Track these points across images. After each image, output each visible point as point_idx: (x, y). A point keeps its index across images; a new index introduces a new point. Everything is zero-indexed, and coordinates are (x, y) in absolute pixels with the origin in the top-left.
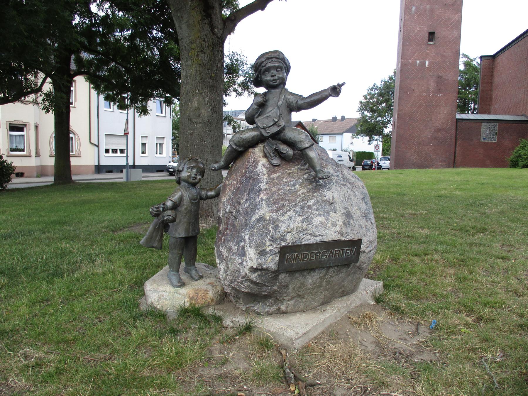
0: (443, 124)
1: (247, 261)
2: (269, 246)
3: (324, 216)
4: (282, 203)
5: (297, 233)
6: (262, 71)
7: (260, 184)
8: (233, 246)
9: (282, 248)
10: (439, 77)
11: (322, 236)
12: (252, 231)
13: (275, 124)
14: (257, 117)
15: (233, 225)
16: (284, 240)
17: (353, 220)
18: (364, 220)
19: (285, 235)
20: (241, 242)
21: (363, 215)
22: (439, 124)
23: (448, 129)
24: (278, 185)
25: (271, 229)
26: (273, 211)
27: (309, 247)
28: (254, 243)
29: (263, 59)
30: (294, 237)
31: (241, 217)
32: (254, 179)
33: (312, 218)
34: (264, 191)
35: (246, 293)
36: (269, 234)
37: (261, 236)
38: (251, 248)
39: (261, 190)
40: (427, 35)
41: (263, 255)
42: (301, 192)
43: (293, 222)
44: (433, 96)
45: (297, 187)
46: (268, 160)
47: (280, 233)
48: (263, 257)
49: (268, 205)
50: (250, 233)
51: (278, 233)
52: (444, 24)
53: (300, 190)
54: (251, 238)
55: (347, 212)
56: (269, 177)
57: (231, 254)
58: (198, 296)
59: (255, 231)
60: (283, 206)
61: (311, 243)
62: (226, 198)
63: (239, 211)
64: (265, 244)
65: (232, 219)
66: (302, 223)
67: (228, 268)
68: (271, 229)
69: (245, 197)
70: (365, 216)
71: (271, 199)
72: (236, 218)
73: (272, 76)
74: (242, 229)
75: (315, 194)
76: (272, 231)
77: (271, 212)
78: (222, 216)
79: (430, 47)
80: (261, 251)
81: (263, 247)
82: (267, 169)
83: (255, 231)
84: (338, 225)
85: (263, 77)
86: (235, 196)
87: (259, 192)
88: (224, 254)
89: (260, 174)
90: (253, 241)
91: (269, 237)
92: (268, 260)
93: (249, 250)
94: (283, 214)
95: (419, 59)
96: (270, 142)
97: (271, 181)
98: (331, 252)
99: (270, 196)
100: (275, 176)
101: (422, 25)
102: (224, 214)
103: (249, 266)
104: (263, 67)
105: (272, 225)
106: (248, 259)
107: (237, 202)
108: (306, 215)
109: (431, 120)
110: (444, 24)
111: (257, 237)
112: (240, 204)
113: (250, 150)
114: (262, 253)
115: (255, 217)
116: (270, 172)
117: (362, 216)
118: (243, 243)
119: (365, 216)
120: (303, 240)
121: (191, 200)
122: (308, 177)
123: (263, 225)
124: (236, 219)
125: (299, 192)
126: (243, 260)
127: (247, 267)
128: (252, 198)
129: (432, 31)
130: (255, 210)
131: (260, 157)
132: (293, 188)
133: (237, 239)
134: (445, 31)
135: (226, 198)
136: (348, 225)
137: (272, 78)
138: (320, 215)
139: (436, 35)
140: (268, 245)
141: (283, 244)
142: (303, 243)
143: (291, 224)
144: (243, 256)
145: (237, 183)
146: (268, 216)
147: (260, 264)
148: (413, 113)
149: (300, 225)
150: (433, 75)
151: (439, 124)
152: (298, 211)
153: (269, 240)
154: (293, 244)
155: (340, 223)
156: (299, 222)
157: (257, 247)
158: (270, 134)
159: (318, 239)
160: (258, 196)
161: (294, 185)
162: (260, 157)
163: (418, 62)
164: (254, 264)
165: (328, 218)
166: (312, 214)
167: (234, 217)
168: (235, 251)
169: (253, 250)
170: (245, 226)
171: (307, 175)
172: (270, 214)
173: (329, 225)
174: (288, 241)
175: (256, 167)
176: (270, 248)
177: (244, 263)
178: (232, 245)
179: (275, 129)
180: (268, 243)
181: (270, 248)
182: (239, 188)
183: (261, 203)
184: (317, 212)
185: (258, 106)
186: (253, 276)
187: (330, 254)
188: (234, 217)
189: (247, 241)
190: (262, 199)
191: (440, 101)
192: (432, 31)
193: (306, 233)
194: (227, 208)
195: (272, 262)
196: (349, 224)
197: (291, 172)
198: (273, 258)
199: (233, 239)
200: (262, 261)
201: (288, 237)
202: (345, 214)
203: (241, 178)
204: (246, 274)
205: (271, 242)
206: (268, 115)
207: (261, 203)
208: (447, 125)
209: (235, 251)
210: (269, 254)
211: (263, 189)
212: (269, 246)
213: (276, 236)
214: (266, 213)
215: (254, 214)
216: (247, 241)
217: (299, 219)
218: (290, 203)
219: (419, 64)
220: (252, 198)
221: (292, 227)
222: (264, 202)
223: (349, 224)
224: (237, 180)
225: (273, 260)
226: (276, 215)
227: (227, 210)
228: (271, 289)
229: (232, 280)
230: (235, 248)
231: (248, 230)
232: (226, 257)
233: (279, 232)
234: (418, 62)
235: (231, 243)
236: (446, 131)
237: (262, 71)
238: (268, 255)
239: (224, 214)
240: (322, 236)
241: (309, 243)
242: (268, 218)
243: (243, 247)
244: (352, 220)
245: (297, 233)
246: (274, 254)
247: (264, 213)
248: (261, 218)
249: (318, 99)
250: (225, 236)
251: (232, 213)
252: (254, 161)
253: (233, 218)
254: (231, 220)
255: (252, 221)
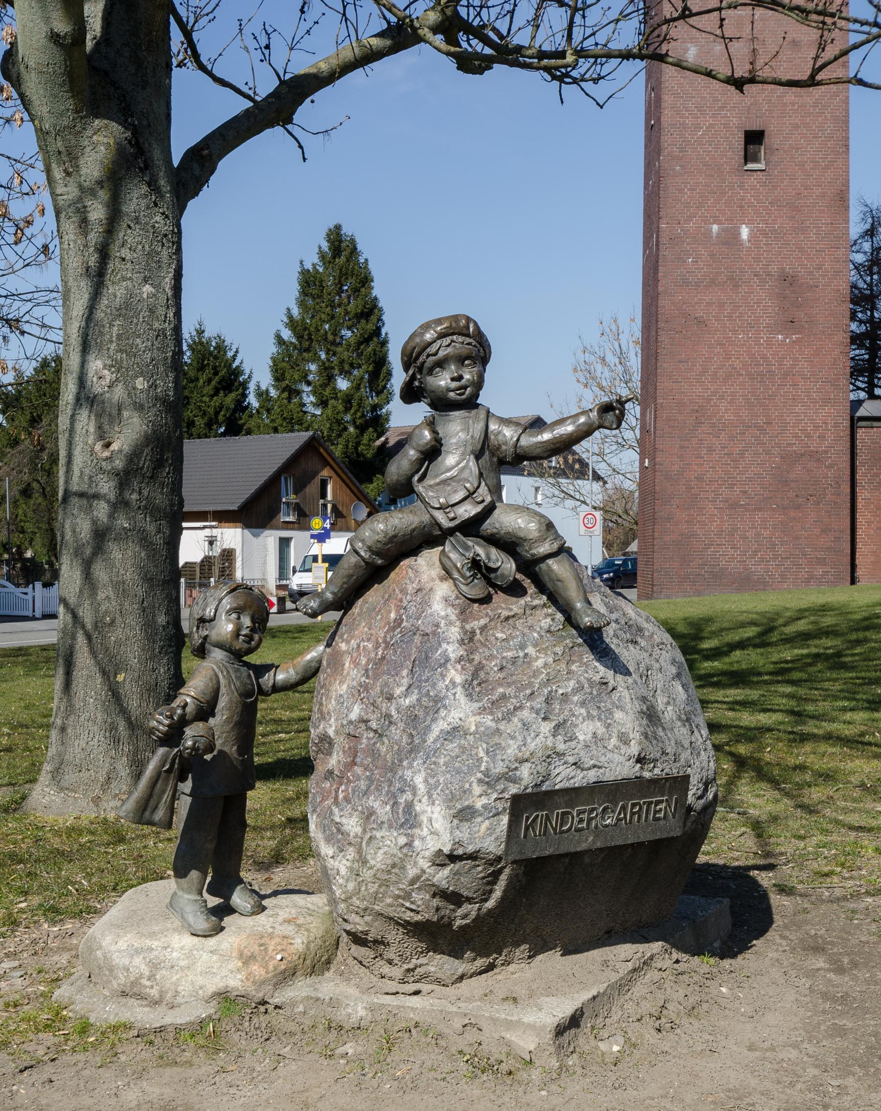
0: (808, 436)
1: (423, 839)
2: (480, 796)
3: (600, 719)
4: (501, 690)
5: (544, 761)
6: (427, 365)
7: (444, 646)
8: (376, 805)
9: (516, 799)
10: (787, 280)
11: (600, 767)
12: (435, 763)
13: (470, 495)
14: (421, 480)
15: (373, 752)
16: (515, 781)
17: (664, 729)
18: (685, 731)
19: (516, 769)
20: (403, 791)
21: (683, 717)
22: (796, 436)
23: (826, 452)
24: (485, 646)
25: (482, 754)
26: (482, 711)
27: (573, 795)
28: (442, 791)
29: (429, 336)
30: (538, 773)
31: (396, 732)
32: (427, 634)
33: (576, 726)
34: (456, 662)
35: (417, 924)
36: (479, 766)
37: (458, 772)
38: (433, 804)
39: (447, 660)
40: (738, 141)
41: (467, 820)
42: (540, 663)
43: (532, 735)
44: (769, 343)
45: (530, 650)
46: (456, 585)
47: (507, 762)
48: (466, 825)
49: (469, 696)
50: (427, 768)
51: (501, 764)
52: (793, 104)
53: (537, 658)
54: (432, 781)
55: (648, 709)
56: (462, 627)
57: (375, 826)
58: (266, 950)
59: (442, 761)
60: (504, 697)
61: (576, 785)
62: (345, 687)
63: (388, 716)
64: (469, 791)
65: (368, 738)
66: (554, 736)
67: (365, 862)
68: (482, 754)
69: (405, 682)
70: (688, 720)
71: (475, 682)
72: (379, 735)
73: (43, 212)
74: (401, 761)
75: (574, 668)
76: (485, 759)
77: (480, 714)
78: (337, 732)
79: (753, 180)
80: (461, 811)
81: (465, 800)
82: (455, 609)
83: (442, 761)
84: (633, 742)
85: (429, 378)
86: (376, 677)
87: (443, 665)
88: (346, 828)
89: (443, 622)
90: (436, 787)
91: (479, 775)
92: (479, 831)
93: (429, 809)
94: (507, 717)
95: (719, 222)
96: (458, 541)
97: (468, 639)
98: (624, 808)
99: (473, 675)
100: (475, 624)
101: (722, 108)
102: (343, 726)
103: (432, 849)
104: (428, 356)
105: (485, 746)
106: (425, 832)
107: (382, 692)
108: (561, 719)
109: (769, 423)
110: (793, 104)
111: (448, 776)
112: (390, 698)
113: (405, 563)
114: (465, 815)
115: (439, 727)
116: (464, 615)
117: (680, 719)
118: (408, 796)
119: (688, 720)
120: (558, 779)
121: (241, 695)
122: (550, 626)
123: (463, 749)
124: (381, 736)
125: (536, 664)
126: (412, 836)
127: (427, 854)
128: (427, 681)
129: (755, 127)
130: (437, 712)
131: (433, 580)
132: (521, 654)
133: (390, 786)
134: (796, 127)
135: (345, 687)
136: (654, 742)
137: (454, 384)
138: (590, 717)
139: (766, 140)
140: (478, 794)
141: (514, 790)
142: (557, 787)
143: (529, 740)
144: (412, 827)
145: (377, 648)
146: (473, 723)
147: (459, 843)
148: (709, 401)
149: (549, 743)
150: (769, 274)
151: (796, 436)
152: (540, 709)
153: (480, 781)
154: (535, 790)
155: (637, 736)
156: (548, 734)
157: (451, 799)
158: (457, 522)
159: (592, 776)
160: (443, 676)
161: (522, 647)
162: (433, 580)
163: (715, 228)
164: (444, 845)
165: (610, 724)
166: (574, 715)
167: (376, 731)
168: (385, 819)
169: (439, 808)
170: (411, 751)
171: (549, 620)
172: (478, 718)
173: (614, 741)
174: (524, 783)
175: (425, 603)
176: (484, 800)
177: (417, 843)
178: (373, 802)
179: (468, 511)
180: (477, 790)
181: (484, 800)
182: (383, 658)
183: (453, 691)
184: (583, 711)
185: (422, 452)
186: (442, 877)
187: (620, 813)
188: (376, 731)
189: (421, 787)
190: (453, 682)
191: (796, 360)
192: (755, 127)
193: (565, 763)
194: (349, 710)
195: (490, 835)
196: (655, 738)
197: (511, 613)
198: (491, 824)
199: (377, 789)
200: (463, 834)
201: (525, 772)
202: (644, 713)
203: (388, 632)
204: (423, 871)
205: (485, 788)
206: (443, 477)
207: (453, 691)
208: (822, 438)
209: (385, 819)
210: (481, 815)
211: (453, 659)
212: (480, 796)
213: (497, 771)
214: (467, 716)
215: (434, 720)
216: (421, 787)
217: (546, 728)
218: (519, 690)
219: (719, 235)
220: (427, 681)
221: (532, 746)
222: (459, 690)
223: (655, 738)
224: (373, 638)
225: (491, 830)
226: (494, 719)
227: (354, 716)
228: (479, 909)
229: (377, 893)
230: (383, 811)
231: (421, 761)
232: (356, 836)
233: (503, 760)
234: (715, 228)
235: (372, 798)
236: (818, 460)
237: (427, 365)
238: (480, 819)
239: (343, 726)
240: (600, 767)
241: (572, 786)
242: (473, 728)
243: (409, 806)
244: (660, 729)
245: (544, 761)
246: (494, 816)
247: (462, 715)
248: (454, 729)
249: (571, 434)
250: (349, 781)
251: (366, 722)
252: (419, 590)
253: (371, 735)
254: (364, 741)
255: (431, 737)
